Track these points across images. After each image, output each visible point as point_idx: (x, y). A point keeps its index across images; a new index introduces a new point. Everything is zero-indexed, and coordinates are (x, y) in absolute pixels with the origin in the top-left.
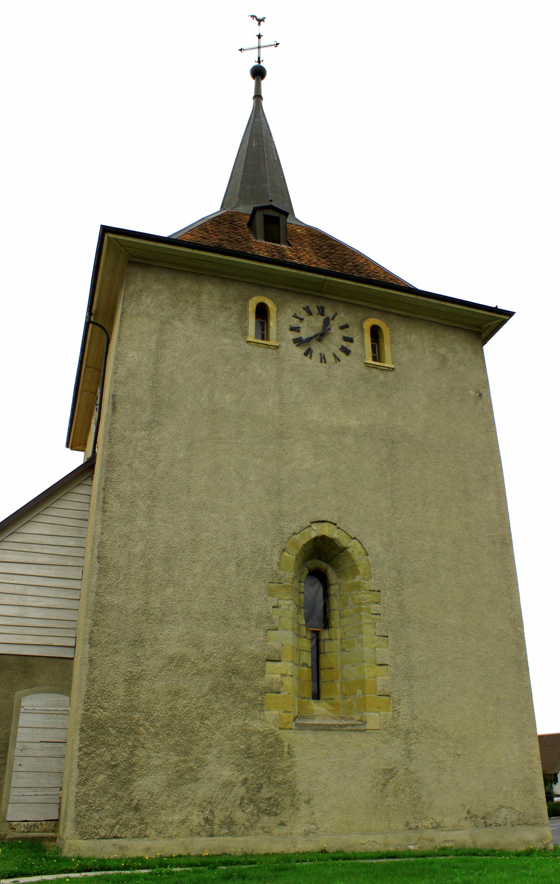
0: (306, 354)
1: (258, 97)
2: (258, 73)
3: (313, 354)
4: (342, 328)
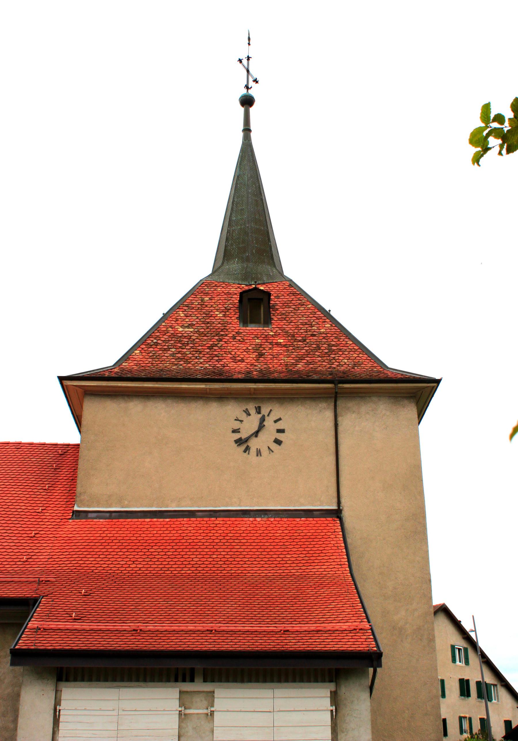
0: (245, 451)
1: (247, 130)
2: (247, 102)
3: (251, 451)
4: (276, 422)
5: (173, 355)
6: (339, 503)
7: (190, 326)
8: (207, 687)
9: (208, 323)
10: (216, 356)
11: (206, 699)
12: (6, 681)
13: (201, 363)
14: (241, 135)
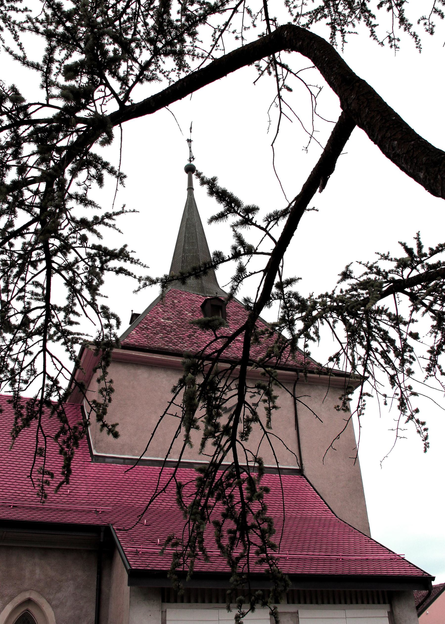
5: (162, 338)
6: (301, 465)
7: (169, 319)
8: (292, 608)
9: (182, 319)
10: (195, 343)
11: (291, 620)
12: (68, 604)
13: (186, 347)
14: (186, 192)
